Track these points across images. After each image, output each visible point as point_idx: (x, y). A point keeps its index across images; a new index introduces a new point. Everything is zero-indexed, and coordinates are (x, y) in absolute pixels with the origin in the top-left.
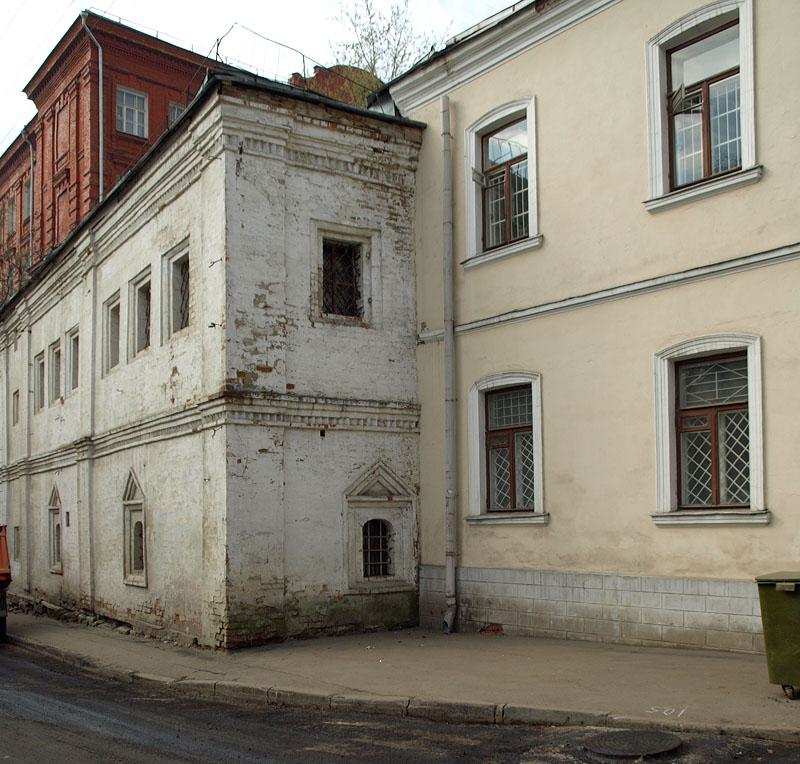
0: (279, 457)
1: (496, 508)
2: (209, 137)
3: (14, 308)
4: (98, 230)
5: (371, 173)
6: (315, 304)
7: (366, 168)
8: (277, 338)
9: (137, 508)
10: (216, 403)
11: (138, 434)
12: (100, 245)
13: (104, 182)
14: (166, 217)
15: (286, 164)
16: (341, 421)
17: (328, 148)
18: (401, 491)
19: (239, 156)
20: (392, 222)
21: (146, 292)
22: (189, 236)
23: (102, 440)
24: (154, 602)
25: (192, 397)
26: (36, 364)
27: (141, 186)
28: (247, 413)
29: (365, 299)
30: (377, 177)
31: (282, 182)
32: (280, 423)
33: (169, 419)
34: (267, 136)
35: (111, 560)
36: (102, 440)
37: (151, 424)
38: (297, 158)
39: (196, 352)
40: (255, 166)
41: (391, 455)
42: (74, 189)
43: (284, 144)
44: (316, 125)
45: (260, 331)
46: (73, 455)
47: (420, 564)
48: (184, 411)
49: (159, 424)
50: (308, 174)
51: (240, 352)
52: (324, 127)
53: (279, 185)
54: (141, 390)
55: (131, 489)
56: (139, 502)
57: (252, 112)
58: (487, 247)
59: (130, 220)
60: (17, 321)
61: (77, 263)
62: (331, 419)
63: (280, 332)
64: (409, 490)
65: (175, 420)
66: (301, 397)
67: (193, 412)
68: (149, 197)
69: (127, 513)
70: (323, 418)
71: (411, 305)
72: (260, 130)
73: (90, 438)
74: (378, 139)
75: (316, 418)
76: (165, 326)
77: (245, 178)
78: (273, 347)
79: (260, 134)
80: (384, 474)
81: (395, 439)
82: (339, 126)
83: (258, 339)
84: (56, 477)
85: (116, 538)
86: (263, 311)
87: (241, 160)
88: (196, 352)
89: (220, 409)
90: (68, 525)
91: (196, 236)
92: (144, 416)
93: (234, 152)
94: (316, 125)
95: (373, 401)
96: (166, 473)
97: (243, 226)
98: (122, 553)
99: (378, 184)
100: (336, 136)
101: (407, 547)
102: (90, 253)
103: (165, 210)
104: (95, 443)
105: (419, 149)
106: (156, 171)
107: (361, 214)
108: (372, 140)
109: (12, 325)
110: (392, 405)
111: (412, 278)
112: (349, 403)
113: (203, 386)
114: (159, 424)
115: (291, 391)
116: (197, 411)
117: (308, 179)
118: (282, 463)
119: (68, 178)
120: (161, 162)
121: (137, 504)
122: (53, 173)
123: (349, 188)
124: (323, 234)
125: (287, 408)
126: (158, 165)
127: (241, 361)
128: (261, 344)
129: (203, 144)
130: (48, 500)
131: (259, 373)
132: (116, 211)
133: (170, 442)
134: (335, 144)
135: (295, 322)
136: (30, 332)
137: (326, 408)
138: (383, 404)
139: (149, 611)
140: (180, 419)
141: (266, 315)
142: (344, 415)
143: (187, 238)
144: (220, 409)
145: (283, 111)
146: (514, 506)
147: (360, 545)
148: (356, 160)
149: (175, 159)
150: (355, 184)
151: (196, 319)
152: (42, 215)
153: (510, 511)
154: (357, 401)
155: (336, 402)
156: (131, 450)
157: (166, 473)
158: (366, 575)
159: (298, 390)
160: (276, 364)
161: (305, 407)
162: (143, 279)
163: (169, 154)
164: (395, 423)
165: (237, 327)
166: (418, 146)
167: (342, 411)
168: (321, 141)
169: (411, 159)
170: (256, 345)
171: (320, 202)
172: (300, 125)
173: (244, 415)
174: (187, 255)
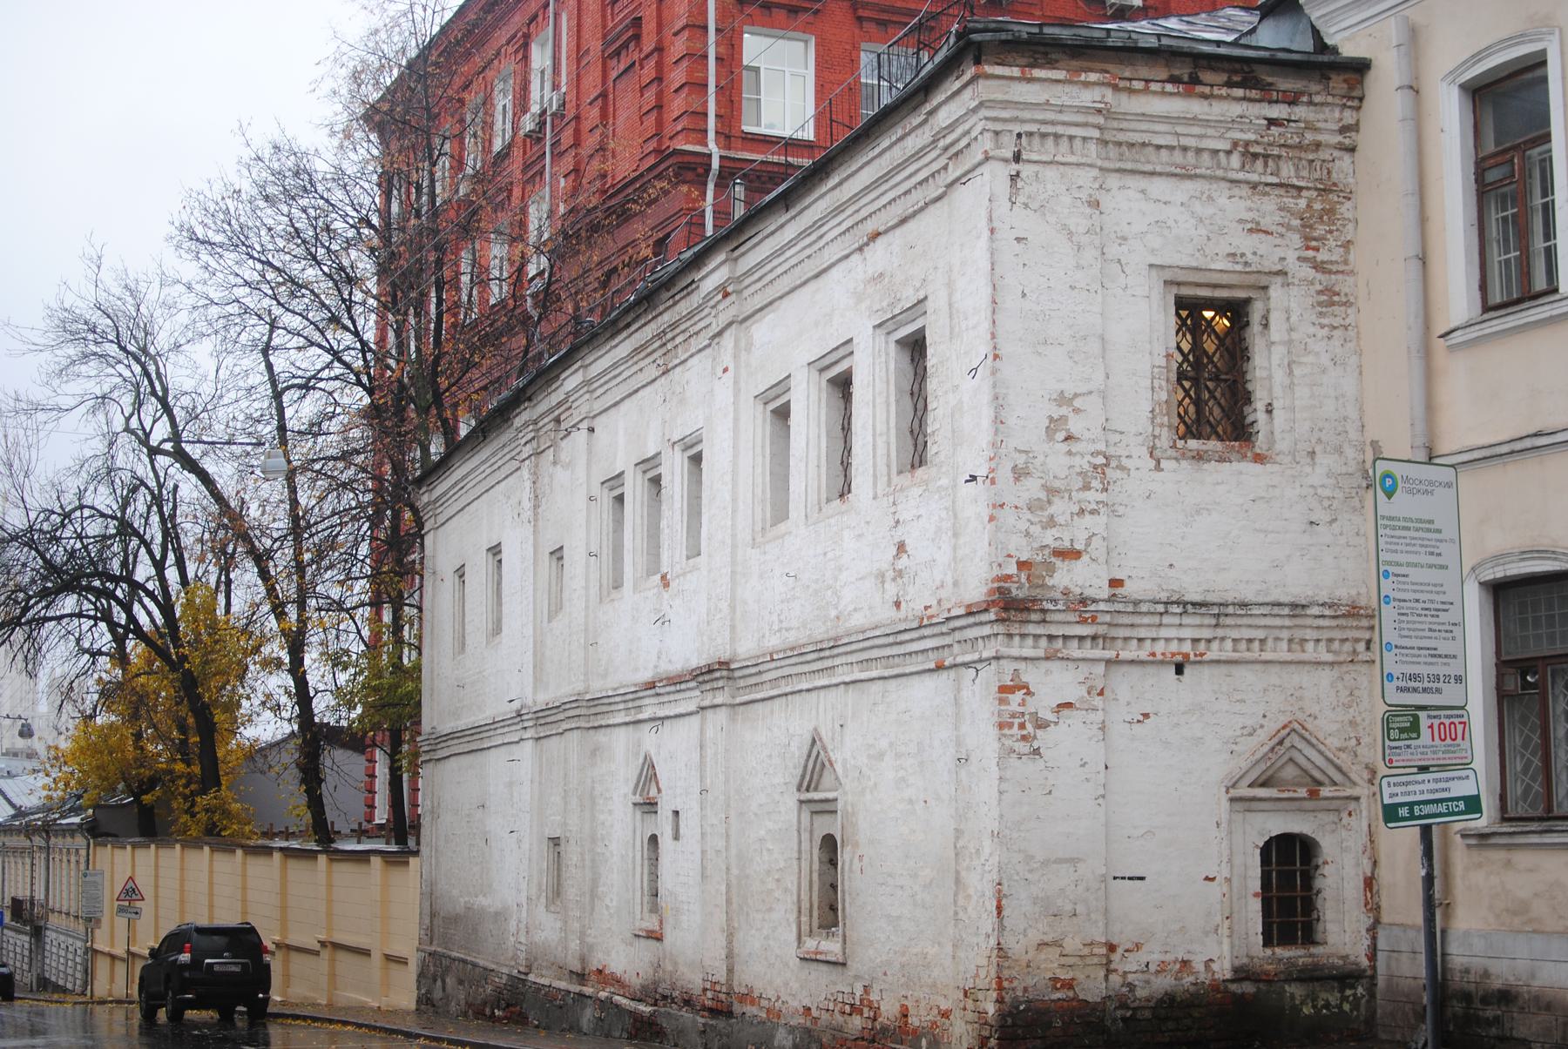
0: (1099, 716)
1: (1521, 812)
2: (959, 131)
3: (558, 376)
4: (743, 254)
5: (1266, 165)
6: (1162, 425)
7: (1255, 156)
8: (1091, 496)
9: (825, 808)
10: (977, 619)
11: (828, 663)
12: (747, 282)
13: (717, 44)
14: (879, 255)
15: (1101, 169)
16: (1215, 645)
17: (1179, 129)
18: (1337, 777)
19: (1014, 167)
20: (1310, 253)
21: (843, 385)
22: (926, 298)
23: (753, 670)
24: (859, 992)
25: (934, 603)
26: (606, 499)
27: (833, 188)
28: (1037, 637)
29: (1260, 405)
30: (1275, 173)
31: (1096, 204)
32: (1098, 653)
33: (891, 639)
34: (1064, 124)
35: (770, 910)
36: (753, 670)
37: (854, 647)
38: (1121, 155)
39: (942, 520)
40: (1047, 183)
41: (1315, 709)
42: (652, 62)
43: (1096, 134)
44: (1155, 93)
45: (1057, 484)
46: (688, 694)
47: (1377, 922)
48: (920, 627)
49: (872, 647)
50: (1143, 182)
51: (1023, 525)
52: (1171, 94)
53: (1088, 211)
54: (836, 579)
55: (815, 770)
56: (830, 795)
57: (1036, 87)
58: (1491, 302)
59: (810, 245)
60: (559, 404)
61: (700, 309)
62: (1195, 641)
63: (1096, 484)
64: (1353, 776)
65: (901, 643)
66: (1136, 603)
67: (936, 630)
68: (848, 212)
69: (806, 816)
70: (1180, 640)
71: (1353, 413)
72: (1050, 116)
73: (727, 663)
74: (1277, 102)
75: (1167, 640)
76: (881, 462)
77: (1026, 206)
78: (1082, 511)
79: (1053, 123)
80: (1301, 745)
81: (1326, 676)
82: (1199, 89)
83: (1056, 500)
84: (649, 740)
85: (782, 864)
86: (1064, 447)
87: (1018, 175)
88: (942, 520)
89: (987, 630)
90: (676, 837)
91: (937, 303)
92: (841, 631)
93: (1006, 161)
94: (1155, 93)
95: (1279, 604)
96: (884, 743)
97: (1024, 295)
98: (795, 898)
99: (1281, 185)
100: (1196, 107)
101: (1352, 889)
102: (726, 295)
103: (880, 240)
104: (737, 674)
105: (1358, 108)
106: (861, 168)
107: (1247, 244)
108: (1265, 105)
109: (551, 410)
110: (1315, 611)
111: (1354, 359)
112: (1230, 610)
113: (956, 584)
114: (872, 647)
115: (1118, 591)
116: (944, 629)
117: (1143, 191)
118: (1103, 728)
119: (637, 37)
120: (871, 154)
121: (827, 801)
122: (604, 27)
123: (1223, 201)
124: (1175, 290)
125: (1110, 625)
126: (865, 159)
127: (1024, 541)
128: (1060, 508)
129: (949, 139)
130: (632, 785)
131: (1058, 562)
132: (782, 226)
133: (893, 683)
134: (1194, 120)
135: (1125, 462)
136: (591, 430)
137: (1186, 620)
138: (1297, 608)
139: (848, 1008)
140: (912, 640)
141: (1070, 453)
142: (1220, 632)
143: (920, 302)
144: (987, 630)
145: (1093, 77)
146: (1549, 808)
147: (1256, 885)
148: (1235, 144)
149: (897, 154)
150: (1236, 191)
151: (942, 457)
152: (577, 118)
153: (1541, 819)
154: (1243, 605)
155: (1203, 610)
156: (814, 694)
157: (884, 743)
158: (1267, 942)
159: (1131, 589)
160: (1088, 545)
161: (1146, 620)
162: (836, 362)
163: (885, 143)
164: (1323, 644)
165: (1017, 479)
166: (1356, 103)
167: (1217, 626)
168: (1166, 119)
169: (1344, 130)
170: (1051, 510)
171: (1166, 232)
172: (1124, 97)
173: (1030, 641)
174: (922, 330)
